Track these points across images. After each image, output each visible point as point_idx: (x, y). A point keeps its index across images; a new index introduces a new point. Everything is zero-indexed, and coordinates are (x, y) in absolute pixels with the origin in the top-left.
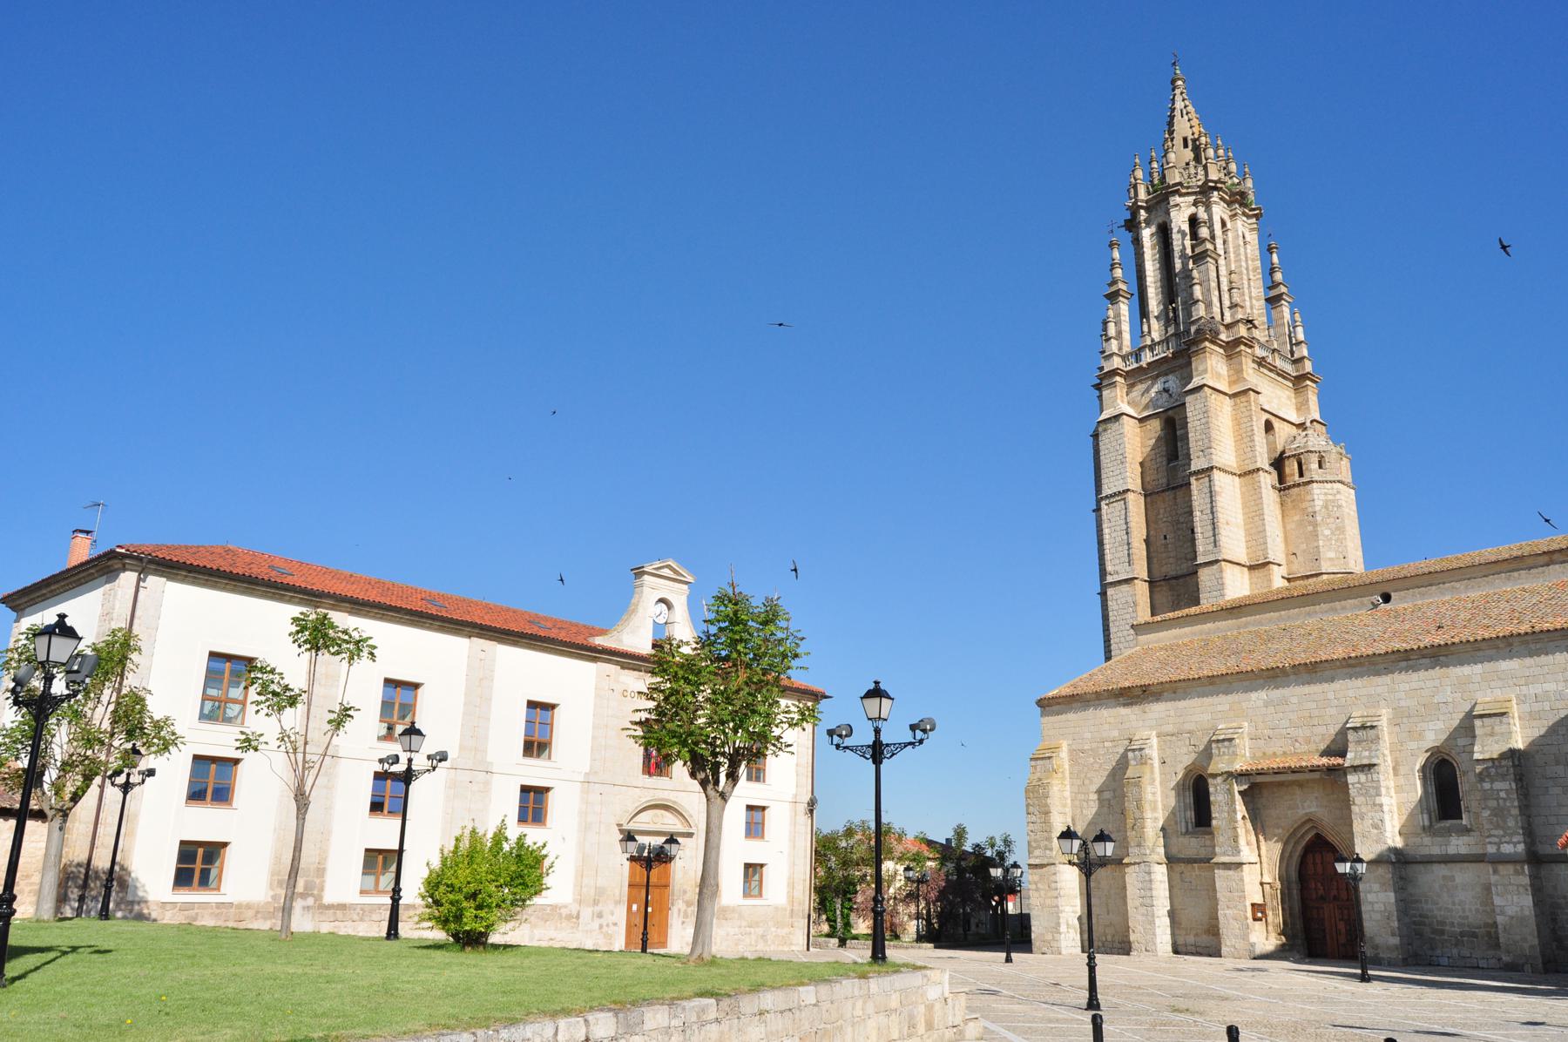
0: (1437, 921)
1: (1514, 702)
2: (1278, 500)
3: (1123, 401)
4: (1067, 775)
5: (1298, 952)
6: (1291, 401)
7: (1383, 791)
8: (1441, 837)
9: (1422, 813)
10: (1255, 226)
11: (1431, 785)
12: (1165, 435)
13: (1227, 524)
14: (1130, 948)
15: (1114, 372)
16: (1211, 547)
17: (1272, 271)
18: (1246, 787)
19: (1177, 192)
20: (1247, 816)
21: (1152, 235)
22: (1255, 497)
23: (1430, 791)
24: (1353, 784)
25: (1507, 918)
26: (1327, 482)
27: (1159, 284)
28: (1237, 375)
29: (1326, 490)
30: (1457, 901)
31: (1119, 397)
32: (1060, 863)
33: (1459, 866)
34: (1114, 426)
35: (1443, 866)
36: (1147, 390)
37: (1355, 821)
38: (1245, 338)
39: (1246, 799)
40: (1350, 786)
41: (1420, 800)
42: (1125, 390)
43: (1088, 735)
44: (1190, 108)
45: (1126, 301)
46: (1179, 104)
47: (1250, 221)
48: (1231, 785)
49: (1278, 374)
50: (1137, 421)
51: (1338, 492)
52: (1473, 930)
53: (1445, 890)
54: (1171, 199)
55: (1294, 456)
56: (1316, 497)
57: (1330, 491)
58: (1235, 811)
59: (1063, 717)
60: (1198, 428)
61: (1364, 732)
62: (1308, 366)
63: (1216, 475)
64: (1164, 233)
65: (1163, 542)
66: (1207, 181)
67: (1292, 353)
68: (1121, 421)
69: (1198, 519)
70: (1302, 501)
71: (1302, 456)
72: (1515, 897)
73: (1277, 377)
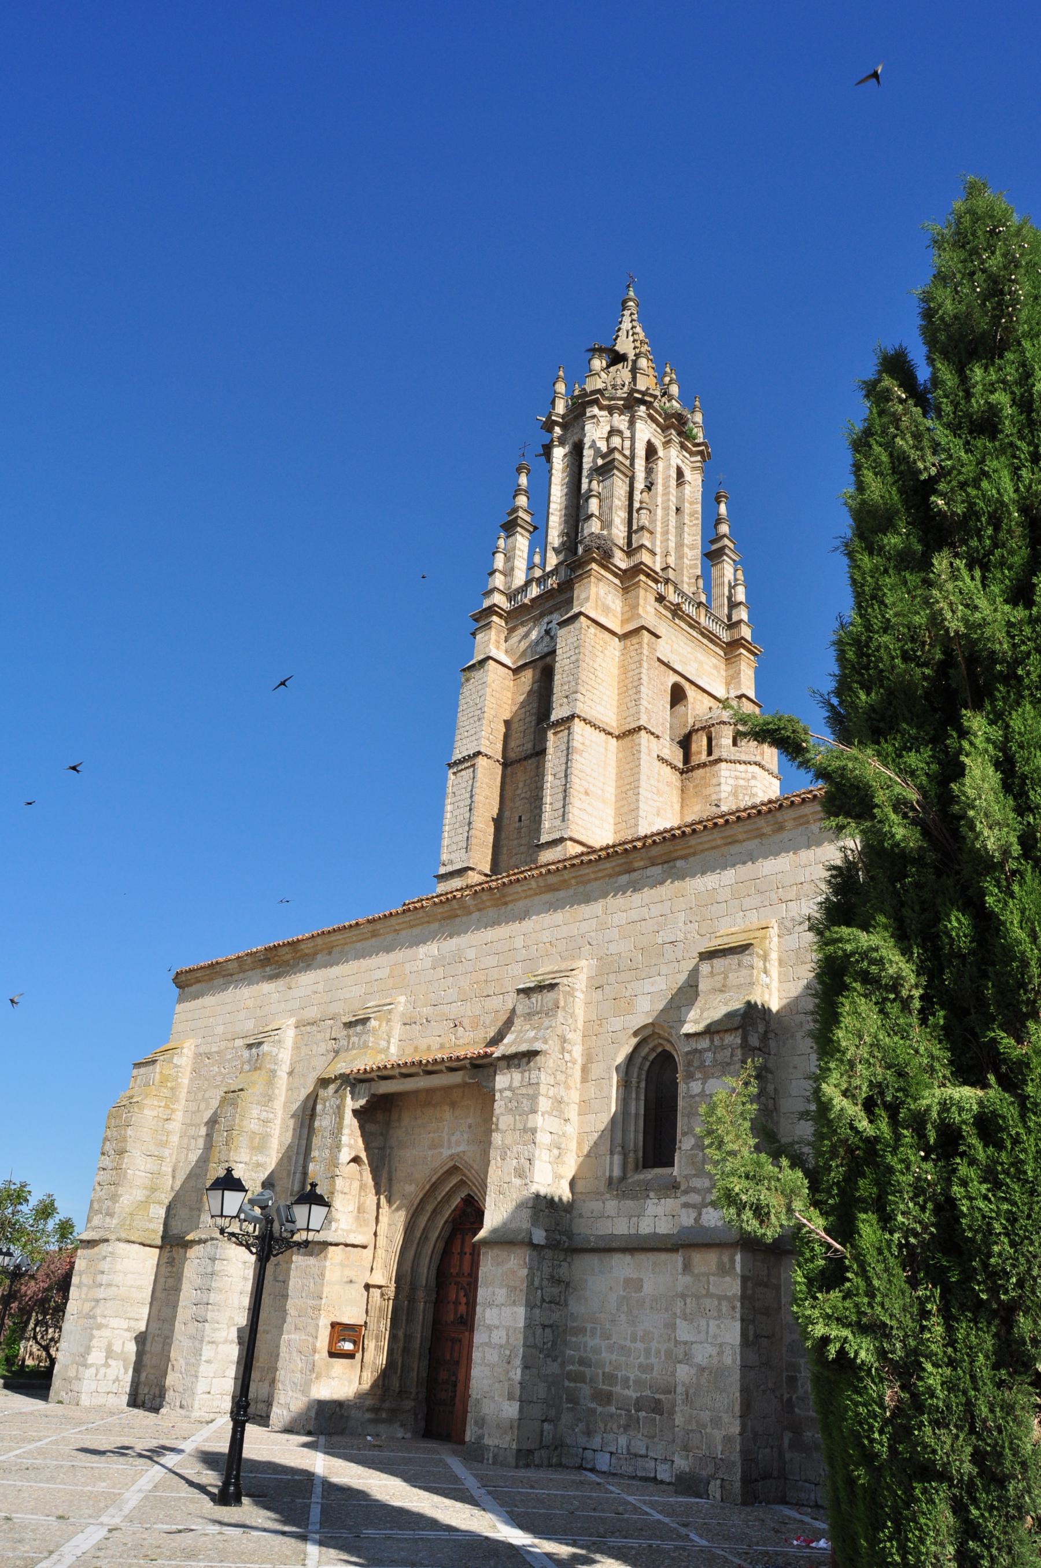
0: (604, 1373)
1: (774, 932)
2: (679, 784)
3: (498, 648)
4: (183, 1094)
5: (402, 1425)
6: (719, 672)
7: (544, 1104)
8: (632, 1199)
9: (612, 1153)
10: (699, 464)
11: (637, 1099)
12: (540, 687)
13: (587, 793)
14: (162, 1396)
15: (491, 610)
16: (558, 822)
17: (718, 521)
18: (362, 1102)
19: (596, 402)
20: (363, 1155)
21: (565, 455)
22: (632, 765)
23: (633, 1111)
24: (501, 1091)
25: (693, 1371)
26: (739, 762)
27: (563, 512)
28: (632, 609)
29: (738, 774)
30: (640, 1334)
31: (492, 641)
32: (119, 1240)
33: (652, 1257)
34: (477, 675)
35: (628, 1258)
36: (527, 635)
37: (493, 1162)
38: (646, 566)
39: (370, 1127)
40: (498, 1096)
41: (613, 1120)
42: (503, 637)
43: (220, 1029)
44: (638, 330)
45: (527, 534)
46: (626, 325)
47: (693, 459)
48: (343, 1099)
49: (703, 634)
50: (511, 672)
51: (754, 777)
52: (657, 1396)
53: (625, 1308)
54: (588, 410)
55: (703, 728)
56: (723, 780)
57: (743, 775)
58: (338, 1147)
59: (200, 1002)
60: (566, 668)
61: (540, 997)
62: (746, 632)
63: (578, 726)
64: (577, 452)
65: (517, 825)
66: (633, 391)
67: (729, 617)
68: (486, 667)
69: (549, 785)
70: (707, 785)
71: (712, 729)
72: (713, 1323)
73: (700, 637)
